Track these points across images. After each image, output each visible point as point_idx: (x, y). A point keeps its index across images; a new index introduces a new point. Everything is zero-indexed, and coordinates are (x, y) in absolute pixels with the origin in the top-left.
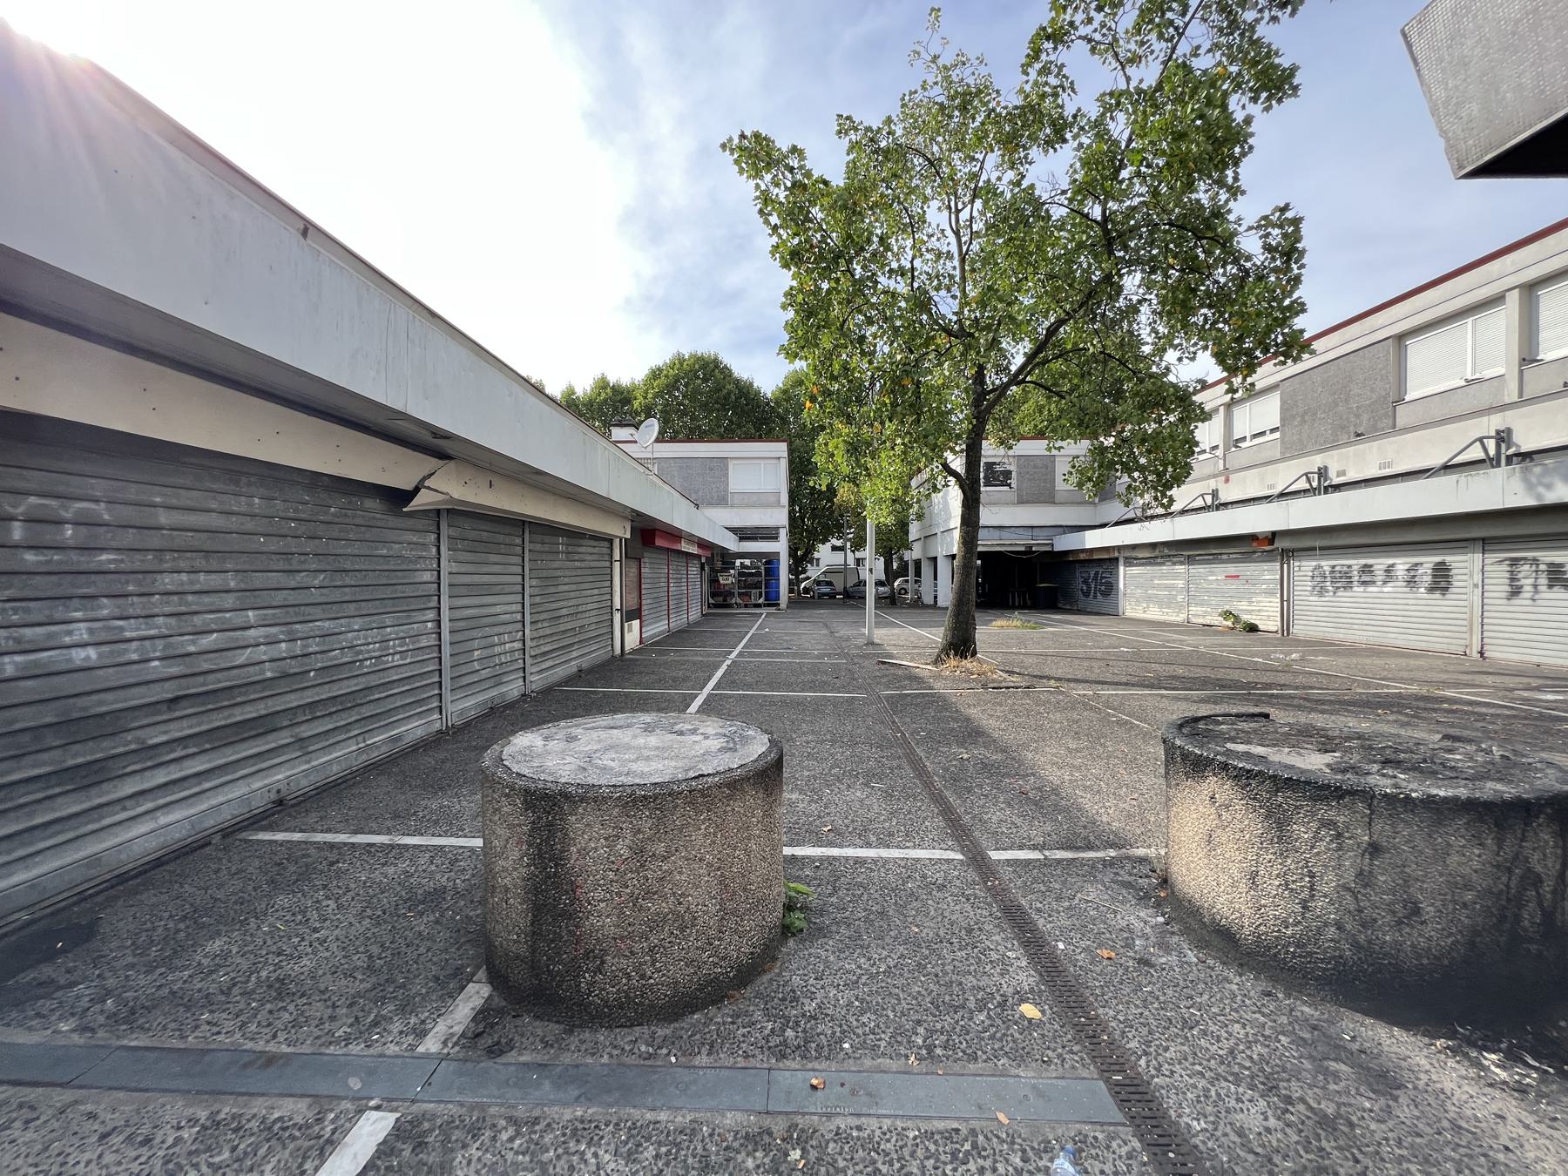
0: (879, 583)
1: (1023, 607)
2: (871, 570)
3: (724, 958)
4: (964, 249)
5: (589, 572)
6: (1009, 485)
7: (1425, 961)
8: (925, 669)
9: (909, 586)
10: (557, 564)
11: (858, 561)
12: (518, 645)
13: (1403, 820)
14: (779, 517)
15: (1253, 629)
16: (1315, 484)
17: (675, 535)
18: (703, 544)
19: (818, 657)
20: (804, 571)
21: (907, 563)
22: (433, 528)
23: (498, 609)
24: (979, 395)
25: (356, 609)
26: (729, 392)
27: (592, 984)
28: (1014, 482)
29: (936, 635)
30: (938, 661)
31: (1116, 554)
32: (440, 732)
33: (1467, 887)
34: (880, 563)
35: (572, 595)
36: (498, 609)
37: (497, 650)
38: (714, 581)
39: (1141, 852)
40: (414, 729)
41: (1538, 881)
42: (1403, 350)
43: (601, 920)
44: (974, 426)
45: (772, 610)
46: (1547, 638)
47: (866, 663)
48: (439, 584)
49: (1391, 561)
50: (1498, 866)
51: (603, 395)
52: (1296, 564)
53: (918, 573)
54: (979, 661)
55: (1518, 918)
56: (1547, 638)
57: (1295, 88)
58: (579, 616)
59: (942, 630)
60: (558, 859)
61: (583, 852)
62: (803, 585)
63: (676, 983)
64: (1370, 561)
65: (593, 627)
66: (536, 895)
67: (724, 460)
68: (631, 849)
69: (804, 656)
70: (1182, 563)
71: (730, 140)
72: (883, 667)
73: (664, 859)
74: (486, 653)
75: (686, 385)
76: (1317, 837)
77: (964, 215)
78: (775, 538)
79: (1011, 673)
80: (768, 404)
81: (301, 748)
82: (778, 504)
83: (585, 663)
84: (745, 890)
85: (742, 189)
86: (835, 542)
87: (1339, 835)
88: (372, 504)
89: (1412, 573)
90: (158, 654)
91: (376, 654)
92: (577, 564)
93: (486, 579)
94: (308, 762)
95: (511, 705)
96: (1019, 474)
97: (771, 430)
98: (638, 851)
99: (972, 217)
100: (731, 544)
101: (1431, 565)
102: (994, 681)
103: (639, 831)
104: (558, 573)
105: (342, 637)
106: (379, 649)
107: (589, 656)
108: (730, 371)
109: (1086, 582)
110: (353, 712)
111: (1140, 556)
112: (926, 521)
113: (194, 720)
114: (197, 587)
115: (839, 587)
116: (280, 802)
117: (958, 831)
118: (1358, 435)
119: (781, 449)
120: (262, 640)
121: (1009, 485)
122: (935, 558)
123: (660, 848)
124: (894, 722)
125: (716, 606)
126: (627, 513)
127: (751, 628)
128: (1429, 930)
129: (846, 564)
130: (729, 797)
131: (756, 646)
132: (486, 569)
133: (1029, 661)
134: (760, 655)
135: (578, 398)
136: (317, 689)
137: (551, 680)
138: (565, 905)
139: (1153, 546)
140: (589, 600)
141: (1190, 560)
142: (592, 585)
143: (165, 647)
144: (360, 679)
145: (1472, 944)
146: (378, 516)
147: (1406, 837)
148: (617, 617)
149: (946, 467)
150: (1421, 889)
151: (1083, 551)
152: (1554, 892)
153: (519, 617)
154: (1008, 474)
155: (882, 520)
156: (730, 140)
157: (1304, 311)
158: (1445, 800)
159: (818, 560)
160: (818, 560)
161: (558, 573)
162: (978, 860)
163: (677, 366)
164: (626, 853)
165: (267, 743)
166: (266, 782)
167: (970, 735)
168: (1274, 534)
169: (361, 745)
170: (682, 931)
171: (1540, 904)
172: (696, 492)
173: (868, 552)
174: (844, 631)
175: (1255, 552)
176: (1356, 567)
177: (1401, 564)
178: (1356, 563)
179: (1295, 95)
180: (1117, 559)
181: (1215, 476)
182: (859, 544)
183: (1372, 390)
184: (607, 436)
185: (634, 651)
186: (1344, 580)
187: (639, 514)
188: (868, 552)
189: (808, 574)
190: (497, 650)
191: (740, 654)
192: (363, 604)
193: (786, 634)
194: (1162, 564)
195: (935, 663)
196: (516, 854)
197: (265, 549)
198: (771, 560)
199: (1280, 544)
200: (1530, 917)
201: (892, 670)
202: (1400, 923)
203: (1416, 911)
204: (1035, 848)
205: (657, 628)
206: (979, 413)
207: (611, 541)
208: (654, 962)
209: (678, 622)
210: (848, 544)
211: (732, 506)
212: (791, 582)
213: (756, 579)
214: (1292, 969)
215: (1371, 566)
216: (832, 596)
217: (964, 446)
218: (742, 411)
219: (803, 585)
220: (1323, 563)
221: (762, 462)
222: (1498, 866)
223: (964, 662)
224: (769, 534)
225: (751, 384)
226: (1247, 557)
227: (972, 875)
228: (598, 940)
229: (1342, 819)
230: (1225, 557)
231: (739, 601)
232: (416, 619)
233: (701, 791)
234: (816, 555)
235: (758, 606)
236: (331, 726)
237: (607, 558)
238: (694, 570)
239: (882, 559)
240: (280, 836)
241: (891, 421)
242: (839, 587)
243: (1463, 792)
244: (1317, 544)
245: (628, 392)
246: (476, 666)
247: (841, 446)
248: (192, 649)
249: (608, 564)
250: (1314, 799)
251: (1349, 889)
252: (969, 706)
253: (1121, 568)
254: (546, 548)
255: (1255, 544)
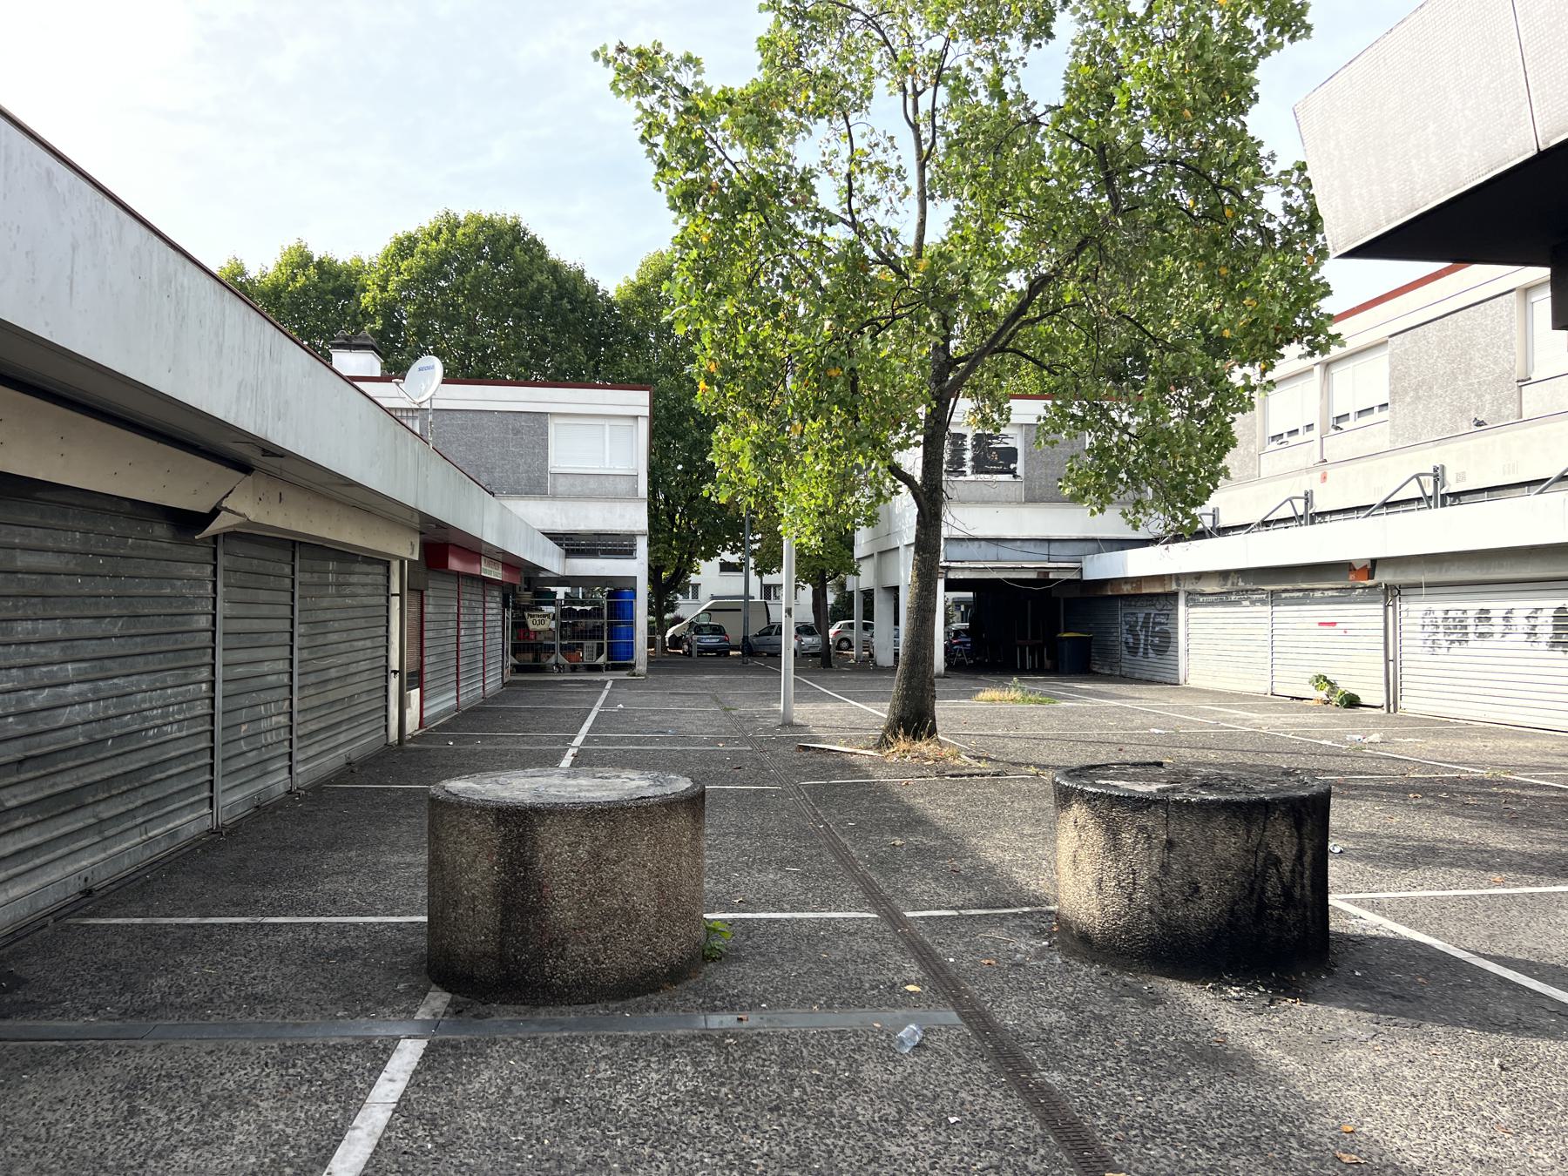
0: (803, 630)
1: (1039, 670)
2: (789, 611)
3: (660, 955)
4: (925, 148)
5: (359, 612)
6: (1013, 472)
7: (1203, 928)
8: (864, 755)
9: (854, 635)
10: (325, 603)
11: (767, 590)
12: (284, 720)
13: (1186, 820)
14: (633, 518)
15: (1352, 702)
16: (1430, 492)
17: (473, 549)
18: (511, 563)
19: (708, 743)
20: (672, 607)
21: (851, 593)
22: (210, 558)
23: (265, 667)
24: (942, 366)
25: (146, 664)
26: (541, 288)
27: (555, 968)
28: (1020, 466)
29: (879, 712)
30: (882, 744)
31: (1174, 587)
32: (210, 831)
33: (1228, 867)
34: (807, 594)
35: (343, 647)
36: (265, 667)
37: (264, 724)
38: (520, 626)
39: (1051, 908)
40: (190, 822)
41: (1277, 862)
42: (1529, 306)
43: (564, 911)
44: (934, 410)
45: (622, 675)
46: (1482, 691)
47: (781, 750)
48: (214, 633)
49: (1510, 605)
50: (1247, 851)
51: (301, 280)
52: (1404, 607)
53: (868, 613)
54: (939, 742)
55: (1263, 890)
56: (1482, 691)
57: (1309, 28)
58: (349, 680)
59: (887, 706)
60: (527, 865)
61: (550, 857)
62: (669, 634)
63: (623, 969)
64: (1485, 605)
65: (364, 698)
66: (505, 898)
67: (540, 419)
68: (589, 853)
69: (686, 740)
70: (1263, 602)
71: (604, 48)
72: (805, 754)
73: (616, 863)
74: (254, 728)
75: (460, 272)
76: (1136, 842)
77: (925, 102)
78: (629, 552)
79: (979, 758)
80: (610, 310)
81: (101, 832)
82: (633, 496)
83: (354, 751)
84: (677, 900)
85: (626, 112)
86: (727, 556)
87: (1149, 837)
88: (161, 530)
89: (1533, 622)
90: (12, 710)
91: (159, 722)
92: (349, 601)
93: (257, 625)
94: (104, 850)
95: (278, 805)
96: (1028, 454)
97: (614, 359)
98: (595, 855)
99: (934, 109)
100: (552, 561)
101: (1551, 612)
102: (954, 767)
103: (596, 839)
104: (329, 615)
105: (132, 697)
106: (162, 716)
107: (354, 743)
108: (542, 248)
109: (1132, 630)
110: (139, 794)
111: (1208, 590)
112: (882, 526)
113: (31, 786)
114: (37, 637)
115: (735, 634)
116: (88, 893)
117: (874, 897)
118: (1479, 424)
119: (638, 401)
120: (77, 698)
121: (1013, 472)
122: (896, 589)
123: (613, 854)
124: (816, 814)
125: (518, 669)
126: (500, 557)
127: (594, 703)
128: (1205, 904)
129: (747, 596)
130: (667, 816)
131: (610, 730)
132: (256, 611)
133: (1012, 745)
134: (620, 741)
135: (252, 282)
136: (113, 762)
137: (322, 772)
138: (533, 902)
139: (1224, 575)
140: (361, 655)
141: (1274, 598)
142: (363, 633)
143: (19, 701)
144: (140, 755)
145: (1232, 912)
146: (165, 545)
147: (1187, 831)
148: (394, 682)
149: (895, 470)
150: (1199, 872)
151: (1126, 580)
152: (1293, 871)
153: (286, 679)
154: (1011, 454)
155: (804, 540)
156: (604, 48)
157: (1328, 293)
158: (1212, 802)
159: (696, 587)
160: (696, 587)
161: (329, 615)
162: (893, 918)
163: (445, 235)
164: (585, 856)
165: (77, 821)
166: (76, 866)
167: (909, 824)
168: (1374, 562)
169: (144, 837)
170: (628, 925)
171: (1280, 879)
172: (490, 471)
173: (783, 577)
174: (745, 708)
175: (1354, 588)
176: (1471, 614)
177: (1521, 605)
178: (1471, 605)
179: (1308, 36)
180: (1175, 595)
181: (1308, 470)
182: (769, 561)
183: (1496, 362)
184: (326, 359)
185: (414, 738)
186: (1457, 631)
187: (426, 519)
188: (783, 577)
189: (679, 612)
190: (264, 724)
191: (587, 740)
192: (150, 657)
193: (655, 712)
194: (1237, 603)
195: (878, 747)
196: (487, 864)
197: (82, 592)
198: (620, 591)
199: (1384, 577)
200: (1272, 888)
201: (818, 758)
202: (1187, 900)
203: (1197, 890)
204: (952, 908)
205: (443, 702)
206: (941, 391)
207: (387, 565)
208: (606, 949)
209: (472, 692)
210: (752, 561)
211: (554, 497)
212: (651, 630)
213: (591, 622)
214: (1124, 953)
215: (1488, 611)
216: (722, 652)
217: (921, 438)
218: (565, 320)
219: (669, 634)
220: (1434, 606)
221: (607, 422)
222: (1247, 851)
223: (918, 745)
224: (619, 545)
225: (581, 273)
226: (1345, 596)
227: (884, 926)
228: (560, 930)
229: (1150, 824)
230: (1318, 594)
231: (562, 660)
232: (193, 679)
233: (645, 808)
234: (693, 578)
235: (596, 669)
236: (122, 809)
237: (382, 590)
238: (494, 606)
239: (809, 588)
240: (103, 921)
241: (814, 420)
242: (735, 634)
243: (1223, 798)
244: (1423, 579)
245: (349, 275)
246: (243, 746)
247: (748, 448)
248: (33, 705)
249: (383, 600)
250: (1134, 810)
251: (1156, 879)
252: (915, 796)
253: (1182, 608)
254: (315, 578)
255: (1352, 576)
